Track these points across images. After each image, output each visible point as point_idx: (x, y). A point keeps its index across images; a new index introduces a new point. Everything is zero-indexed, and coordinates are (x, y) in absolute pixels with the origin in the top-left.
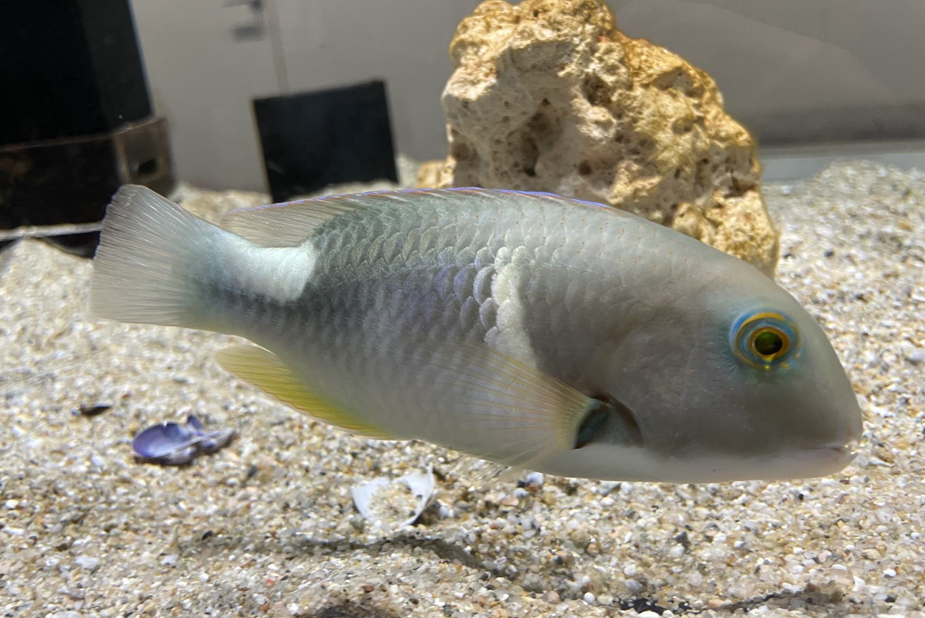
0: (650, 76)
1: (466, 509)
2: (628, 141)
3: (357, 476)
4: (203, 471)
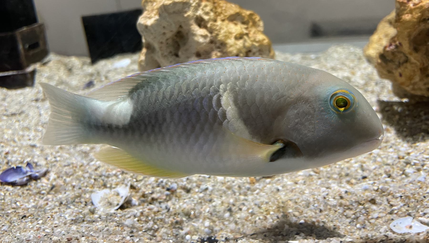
0: (226, 16)
1: (144, 202)
2: (216, 43)
3: (96, 189)
4: (31, 188)
